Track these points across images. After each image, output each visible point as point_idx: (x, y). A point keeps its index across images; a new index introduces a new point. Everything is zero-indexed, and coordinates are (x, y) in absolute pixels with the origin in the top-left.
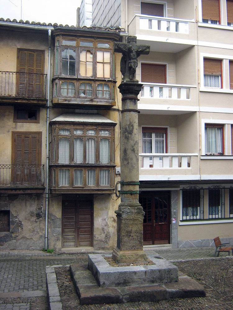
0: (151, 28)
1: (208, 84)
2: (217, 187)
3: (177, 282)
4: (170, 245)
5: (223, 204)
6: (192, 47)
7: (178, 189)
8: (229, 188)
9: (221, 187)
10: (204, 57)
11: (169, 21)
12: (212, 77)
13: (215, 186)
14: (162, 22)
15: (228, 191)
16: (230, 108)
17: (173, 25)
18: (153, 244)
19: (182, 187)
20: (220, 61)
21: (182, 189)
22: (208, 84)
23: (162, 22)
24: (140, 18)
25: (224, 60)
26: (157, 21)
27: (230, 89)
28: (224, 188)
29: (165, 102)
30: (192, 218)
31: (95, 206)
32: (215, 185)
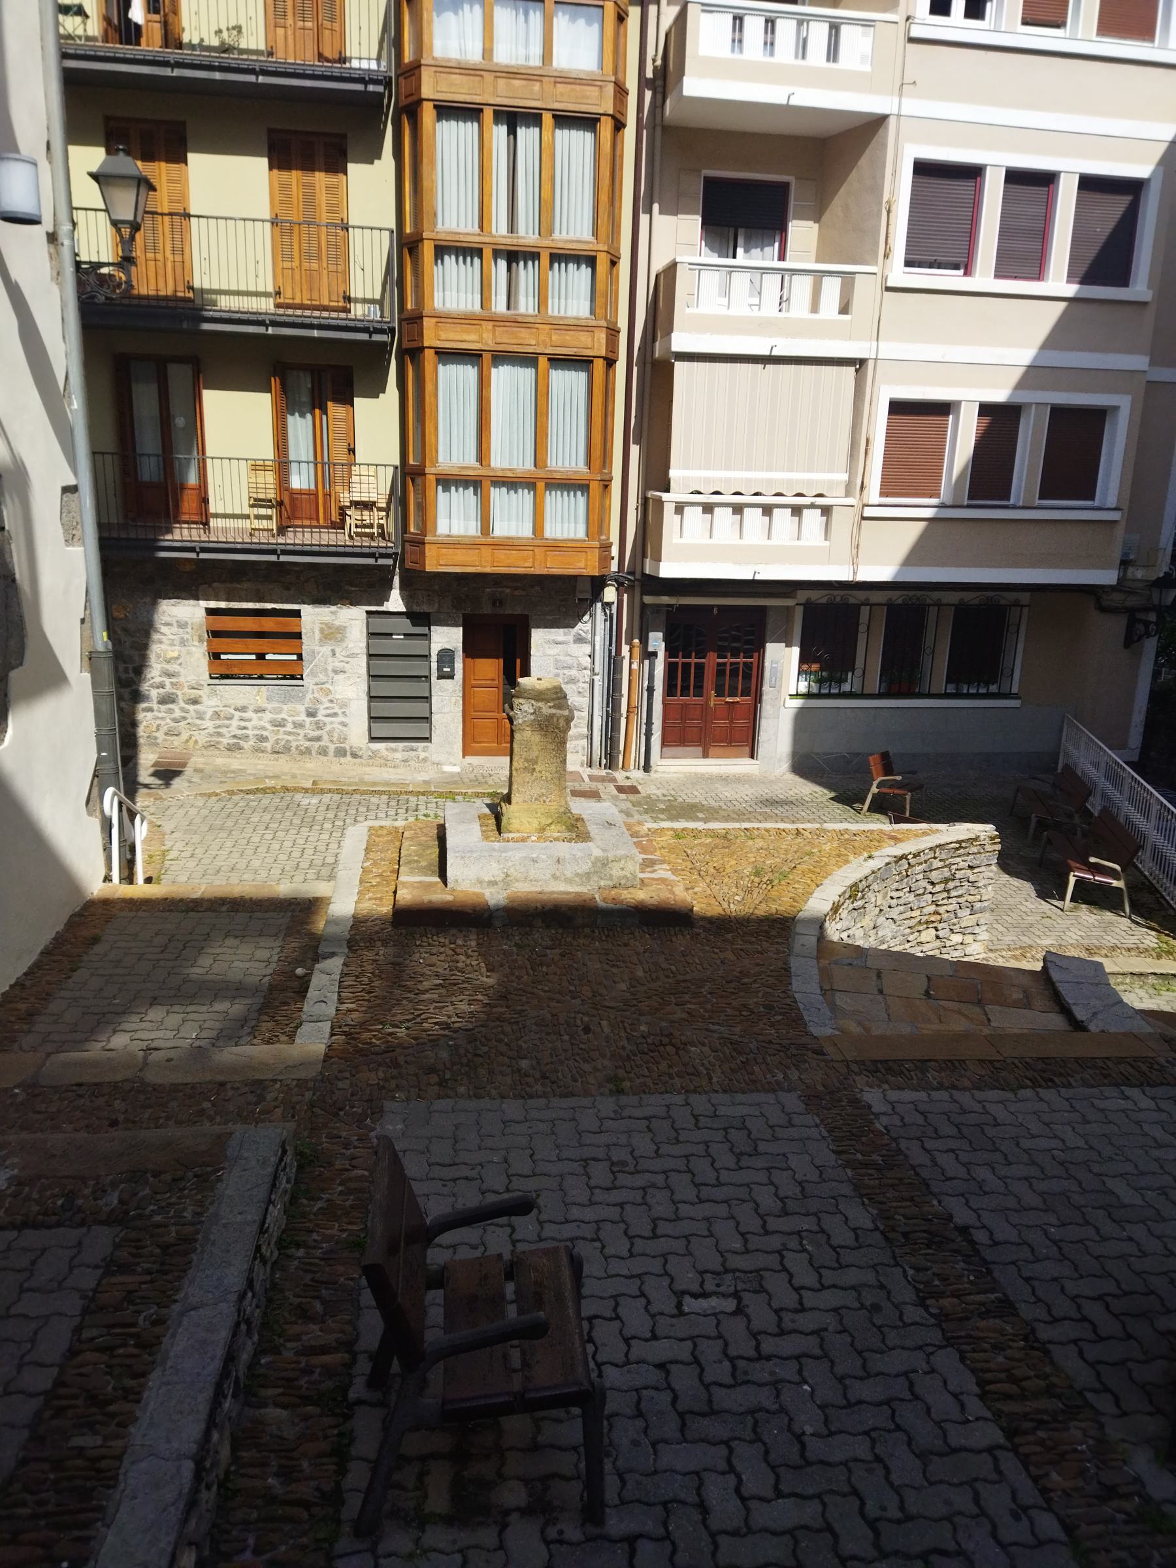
0: (804, 57)
4: (754, 762)
6: (880, 121)
7: (790, 602)
9: (929, 601)
11: (802, 21)
14: (845, 30)
15: (950, 613)
17: (818, 34)
18: (705, 755)
19: (803, 596)
20: (974, 173)
21: (803, 601)
23: (781, 24)
24: (703, 11)
25: (1062, 175)
26: (827, 25)
27: (1068, 282)
28: (939, 604)
29: (762, 327)
30: (826, 691)
32: (911, 593)
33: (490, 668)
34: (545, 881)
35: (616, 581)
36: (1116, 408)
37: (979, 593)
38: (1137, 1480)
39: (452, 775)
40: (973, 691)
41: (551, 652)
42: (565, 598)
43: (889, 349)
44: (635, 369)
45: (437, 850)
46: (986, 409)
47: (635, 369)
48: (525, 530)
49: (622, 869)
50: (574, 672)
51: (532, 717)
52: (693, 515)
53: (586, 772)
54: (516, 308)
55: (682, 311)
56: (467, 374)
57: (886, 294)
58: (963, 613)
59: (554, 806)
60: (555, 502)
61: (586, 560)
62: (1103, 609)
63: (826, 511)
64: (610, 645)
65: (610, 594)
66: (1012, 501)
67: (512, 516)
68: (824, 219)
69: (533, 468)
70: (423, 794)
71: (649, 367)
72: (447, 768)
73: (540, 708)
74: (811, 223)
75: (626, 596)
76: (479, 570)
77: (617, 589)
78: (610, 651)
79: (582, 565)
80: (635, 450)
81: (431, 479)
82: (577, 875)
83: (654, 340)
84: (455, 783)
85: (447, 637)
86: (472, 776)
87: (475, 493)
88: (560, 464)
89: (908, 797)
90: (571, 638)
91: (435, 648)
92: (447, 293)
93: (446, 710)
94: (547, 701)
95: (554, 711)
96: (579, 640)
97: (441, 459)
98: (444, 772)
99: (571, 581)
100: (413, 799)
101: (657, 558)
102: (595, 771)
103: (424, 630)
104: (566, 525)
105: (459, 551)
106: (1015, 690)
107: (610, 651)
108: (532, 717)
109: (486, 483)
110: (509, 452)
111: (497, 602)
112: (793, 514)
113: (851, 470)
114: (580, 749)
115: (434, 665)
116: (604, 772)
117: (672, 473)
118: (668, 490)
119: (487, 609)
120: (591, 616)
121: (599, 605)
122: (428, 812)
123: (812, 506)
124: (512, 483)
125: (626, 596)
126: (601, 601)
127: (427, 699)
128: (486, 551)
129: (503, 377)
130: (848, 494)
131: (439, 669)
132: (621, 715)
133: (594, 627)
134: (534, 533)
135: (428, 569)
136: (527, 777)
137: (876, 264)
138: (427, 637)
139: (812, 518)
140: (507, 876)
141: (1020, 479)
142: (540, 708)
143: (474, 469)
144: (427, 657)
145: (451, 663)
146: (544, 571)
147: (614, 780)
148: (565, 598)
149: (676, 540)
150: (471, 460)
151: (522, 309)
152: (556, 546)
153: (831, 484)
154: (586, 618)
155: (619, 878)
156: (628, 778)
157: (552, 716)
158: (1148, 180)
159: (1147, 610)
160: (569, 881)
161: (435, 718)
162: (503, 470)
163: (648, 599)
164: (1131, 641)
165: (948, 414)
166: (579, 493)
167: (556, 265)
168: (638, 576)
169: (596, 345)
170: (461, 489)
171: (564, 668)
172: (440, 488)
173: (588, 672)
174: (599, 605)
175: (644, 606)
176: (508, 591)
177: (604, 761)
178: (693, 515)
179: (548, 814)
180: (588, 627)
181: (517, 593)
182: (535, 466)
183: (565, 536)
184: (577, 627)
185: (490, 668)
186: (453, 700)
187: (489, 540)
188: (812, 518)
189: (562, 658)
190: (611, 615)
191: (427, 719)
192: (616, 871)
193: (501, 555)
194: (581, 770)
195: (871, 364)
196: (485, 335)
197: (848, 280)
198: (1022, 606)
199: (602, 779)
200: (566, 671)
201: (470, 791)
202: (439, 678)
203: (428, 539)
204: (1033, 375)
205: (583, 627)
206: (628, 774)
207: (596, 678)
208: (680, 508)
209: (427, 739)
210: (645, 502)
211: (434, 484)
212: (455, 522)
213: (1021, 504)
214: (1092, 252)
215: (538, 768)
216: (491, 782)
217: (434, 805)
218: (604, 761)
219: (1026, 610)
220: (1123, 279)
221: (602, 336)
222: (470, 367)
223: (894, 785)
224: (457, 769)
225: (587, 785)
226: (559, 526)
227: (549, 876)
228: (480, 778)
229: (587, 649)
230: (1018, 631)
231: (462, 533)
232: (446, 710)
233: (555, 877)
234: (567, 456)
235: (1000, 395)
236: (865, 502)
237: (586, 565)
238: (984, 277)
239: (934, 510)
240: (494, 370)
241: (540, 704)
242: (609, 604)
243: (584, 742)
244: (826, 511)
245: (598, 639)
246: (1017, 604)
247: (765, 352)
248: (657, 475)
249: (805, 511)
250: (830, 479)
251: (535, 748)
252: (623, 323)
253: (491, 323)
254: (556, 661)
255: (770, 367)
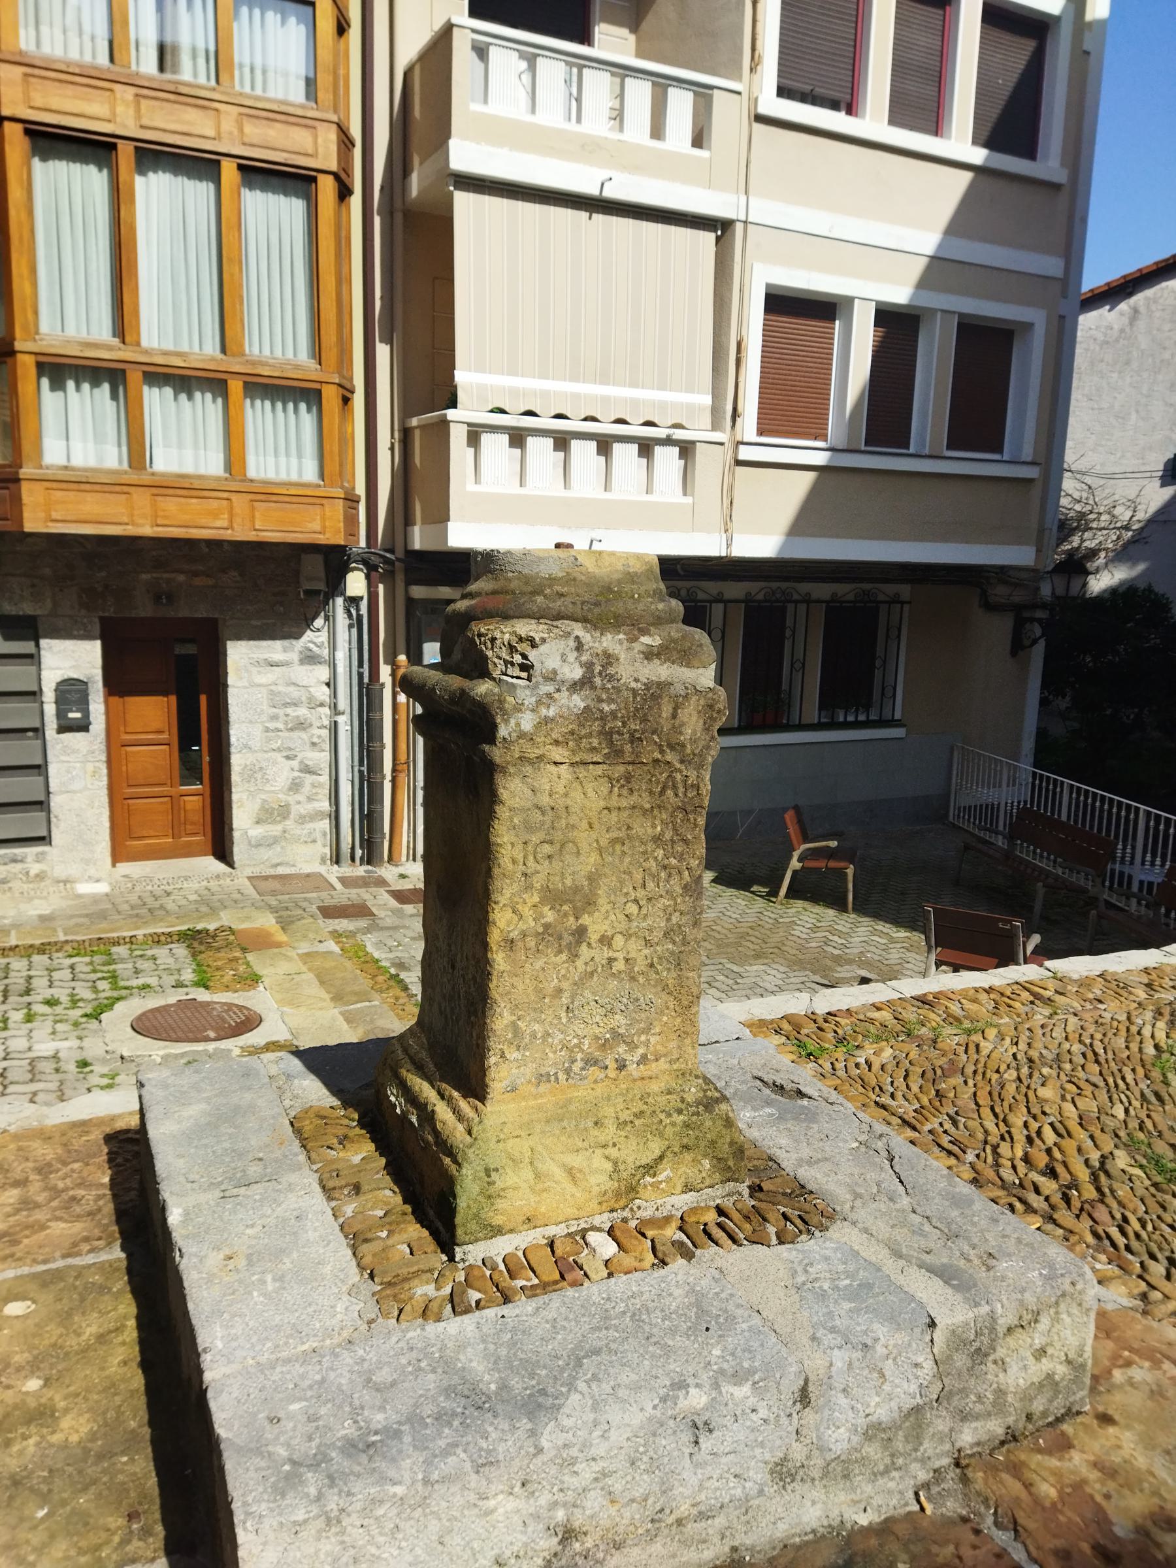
1: (1071, 793)
2: (778, 596)
3: (552, 1242)
5: (798, 665)
8: (827, 602)
10: (768, 286)
12: (95, 384)
13: (774, 593)
16: (1027, 544)
22: (1071, 793)
28: (808, 600)
29: (588, 149)
31: (160, 698)
33: (154, 713)
34: (745, 1505)
35: (365, 562)
36: (1028, 327)
37: (853, 586)
38: (144, 935)
39: (95, 899)
40: (851, 718)
41: (262, 679)
42: (281, 584)
43: (762, 210)
44: (377, 220)
45: (127, 1308)
46: (886, 316)
47: (377, 220)
48: (212, 464)
49: (1041, 1353)
50: (302, 712)
51: (578, 702)
52: (495, 445)
53: (333, 873)
54: (176, 69)
55: (465, 104)
56: (86, 182)
57: (758, 127)
58: (835, 612)
59: (659, 1078)
60: (263, 421)
61: (323, 519)
62: (989, 607)
63: (686, 450)
64: (361, 665)
65: (356, 583)
66: (912, 450)
67: (184, 438)
68: (645, 26)
69: (218, 353)
70: (42, 949)
71: (399, 218)
72: (84, 888)
73: (609, 659)
74: (624, 32)
75: (381, 587)
76: (130, 530)
77: (368, 577)
78: (361, 675)
79: (316, 526)
80: (383, 352)
81: (26, 364)
82: (874, 1431)
83: (406, 172)
84: (102, 916)
85: (72, 659)
86: (133, 899)
87: (114, 396)
88: (267, 352)
89: (850, 871)
90: (294, 656)
91: (50, 678)
92: (45, 29)
93: (77, 785)
94: (634, 625)
95: (662, 671)
96: (310, 658)
97: (45, 327)
98: (79, 896)
99: (293, 554)
100: (18, 965)
101: (440, 515)
102: (347, 870)
103: (26, 647)
104: (283, 459)
105: (89, 497)
106: (898, 716)
107: (361, 675)
108: (578, 702)
109: (135, 376)
110: (173, 322)
111: (161, 596)
112: (640, 455)
113: (717, 392)
114: (318, 835)
115: (50, 709)
116: (361, 870)
117: (460, 376)
118: (453, 404)
119: (144, 609)
120: (327, 618)
121: (340, 601)
122: (56, 992)
123: (668, 441)
124: (183, 381)
125: (381, 587)
126: (343, 593)
127: (40, 769)
128: (141, 498)
129: (158, 195)
130: (715, 426)
131: (60, 715)
132: (383, 777)
133: (332, 637)
134: (228, 466)
135: (29, 526)
136: (554, 967)
137: (739, 78)
138: (33, 658)
139: (667, 459)
140: (568, 1535)
141: (924, 414)
142: (609, 659)
143: (110, 348)
144: (34, 695)
145: (83, 702)
146: (251, 536)
147: (382, 882)
148: (281, 584)
149: (471, 487)
150: (101, 329)
151: (186, 75)
152: (267, 493)
153: (691, 408)
154: (319, 622)
155: (1026, 1397)
156: (402, 876)
157: (655, 692)
158: (1057, 19)
159: (1034, 606)
160: (841, 1470)
161: (56, 802)
162: (166, 353)
163: (419, 592)
164: (1018, 646)
165: (833, 319)
166: (303, 406)
167: (244, 10)
168: (400, 553)
169: (322, 151)
170: (86, 386)
171: (286, 705)
172: (45, 382)
173: (327, 710)
174: (340, 601)
175: (410, 602)
176: (181, 578)
177: (359, 853)
178: (495, 445)
179: (639, 1121)
180: (323, 637)
181: (198, 581)
182: (224, 350)
183: (283, 477)
184: (305, 638)
185: (154, 713)
186: (90, 767)
187: (145, 479)
188: (667, 459)
189: (281, 688)
190: (360, 617)
191: (42, 805)
192: (1019, 1371)
193: (170, 506)
194: (322, 870)
195: (739, 227)
196: (120, 109)
197: (703, 95)
198: (902, 603)
199: (364, 882)
200: (289, 711)
201: (140, 933)
202: (62, 729)
203: (25, 472)
204: (939, 270)
205: (315, 637)
206: (401, 870)
207: (343, 720)
208: (474, 438)
209: (44, 840)
210: (405, 436)
211: (33, 371)
212: (77, 446)
213: (927, 451)
214: (994, 113)
215: (596, 925)
216: (171, 906)
217: (66, 974)
218: (359, 853)
219: (906, 607)
220: (1029, 151)
221: (329, 137)
222: (92, 169)
223: (830, 854)
224: (103, 888)
225: (343, 895)
226: (271, 460)
227: (758, 1475)
228: (150, 901)
229: (323, 673)
230: (899, 636)
231: (92, 463)
232: (77, 785)
233: (784, 1473)
234: (278, 336)
235: (900, 295)
236: (739, 438)
237: (321, 527)
238: (873, 121)
239: (827, 454)
240: (139, 181)
241: (610, 642)
242: (354, 601)
243: (325, 824)
244: (686, 450)
245: (341, 656)
246: (896, 600)
247: (592, 190)
248: (429, 383)
249: (658, 450)
250: (686, 402)
251: (584, 838)
252: (356, 132)
253: (132, 91)
254: (272, 693)
255: (598, 218)
